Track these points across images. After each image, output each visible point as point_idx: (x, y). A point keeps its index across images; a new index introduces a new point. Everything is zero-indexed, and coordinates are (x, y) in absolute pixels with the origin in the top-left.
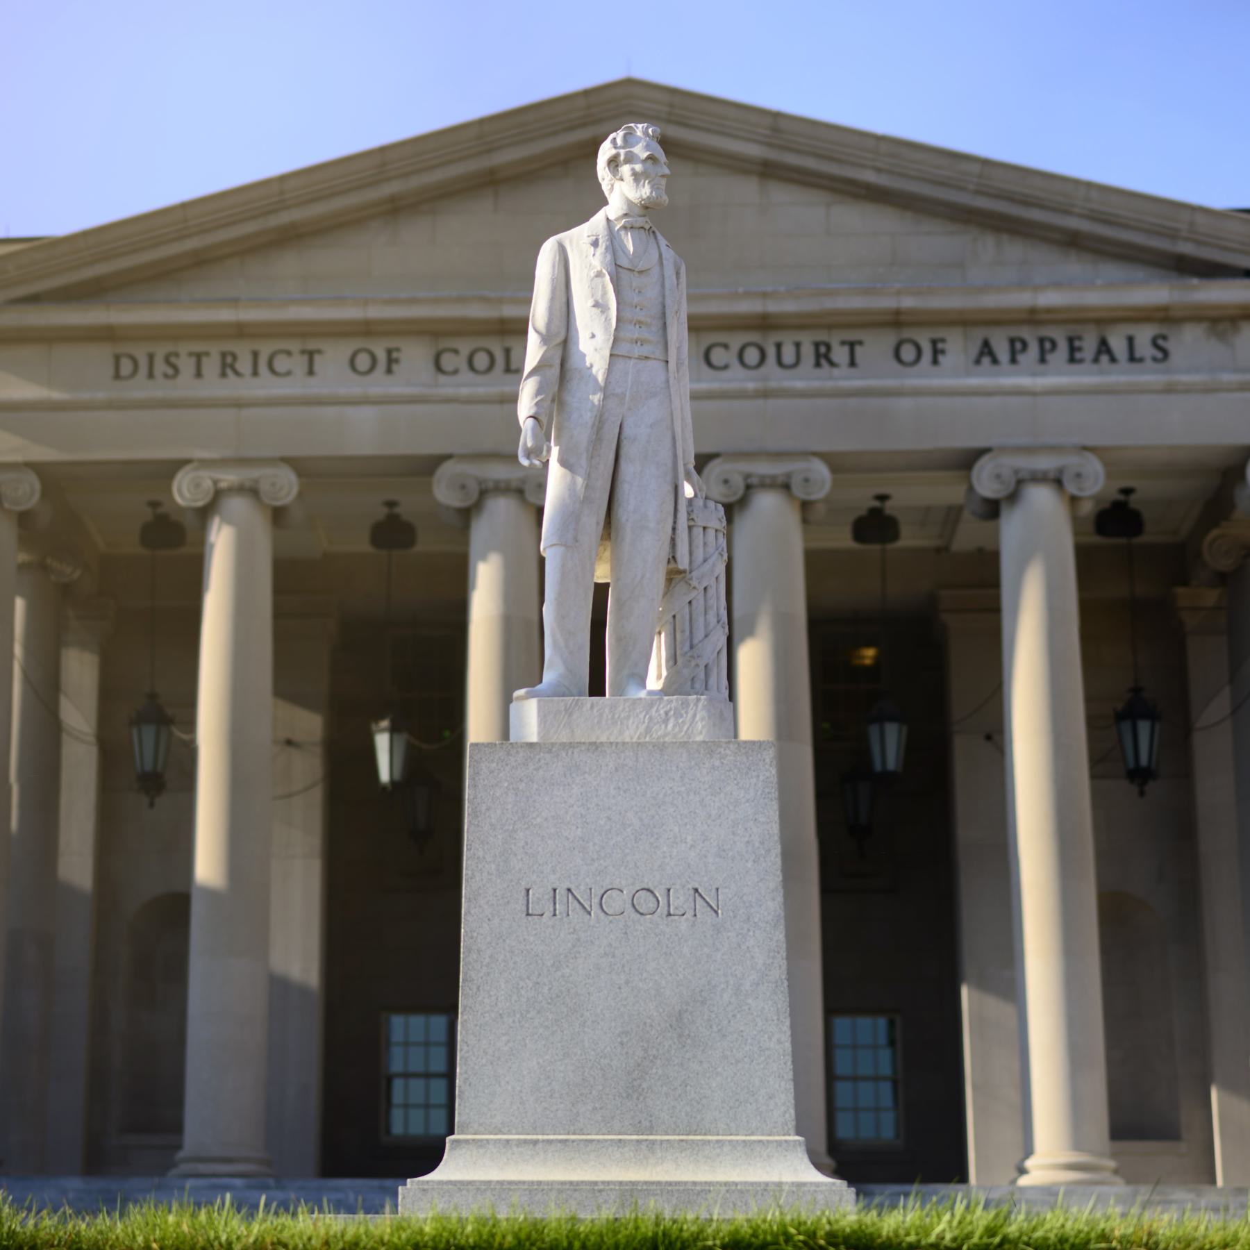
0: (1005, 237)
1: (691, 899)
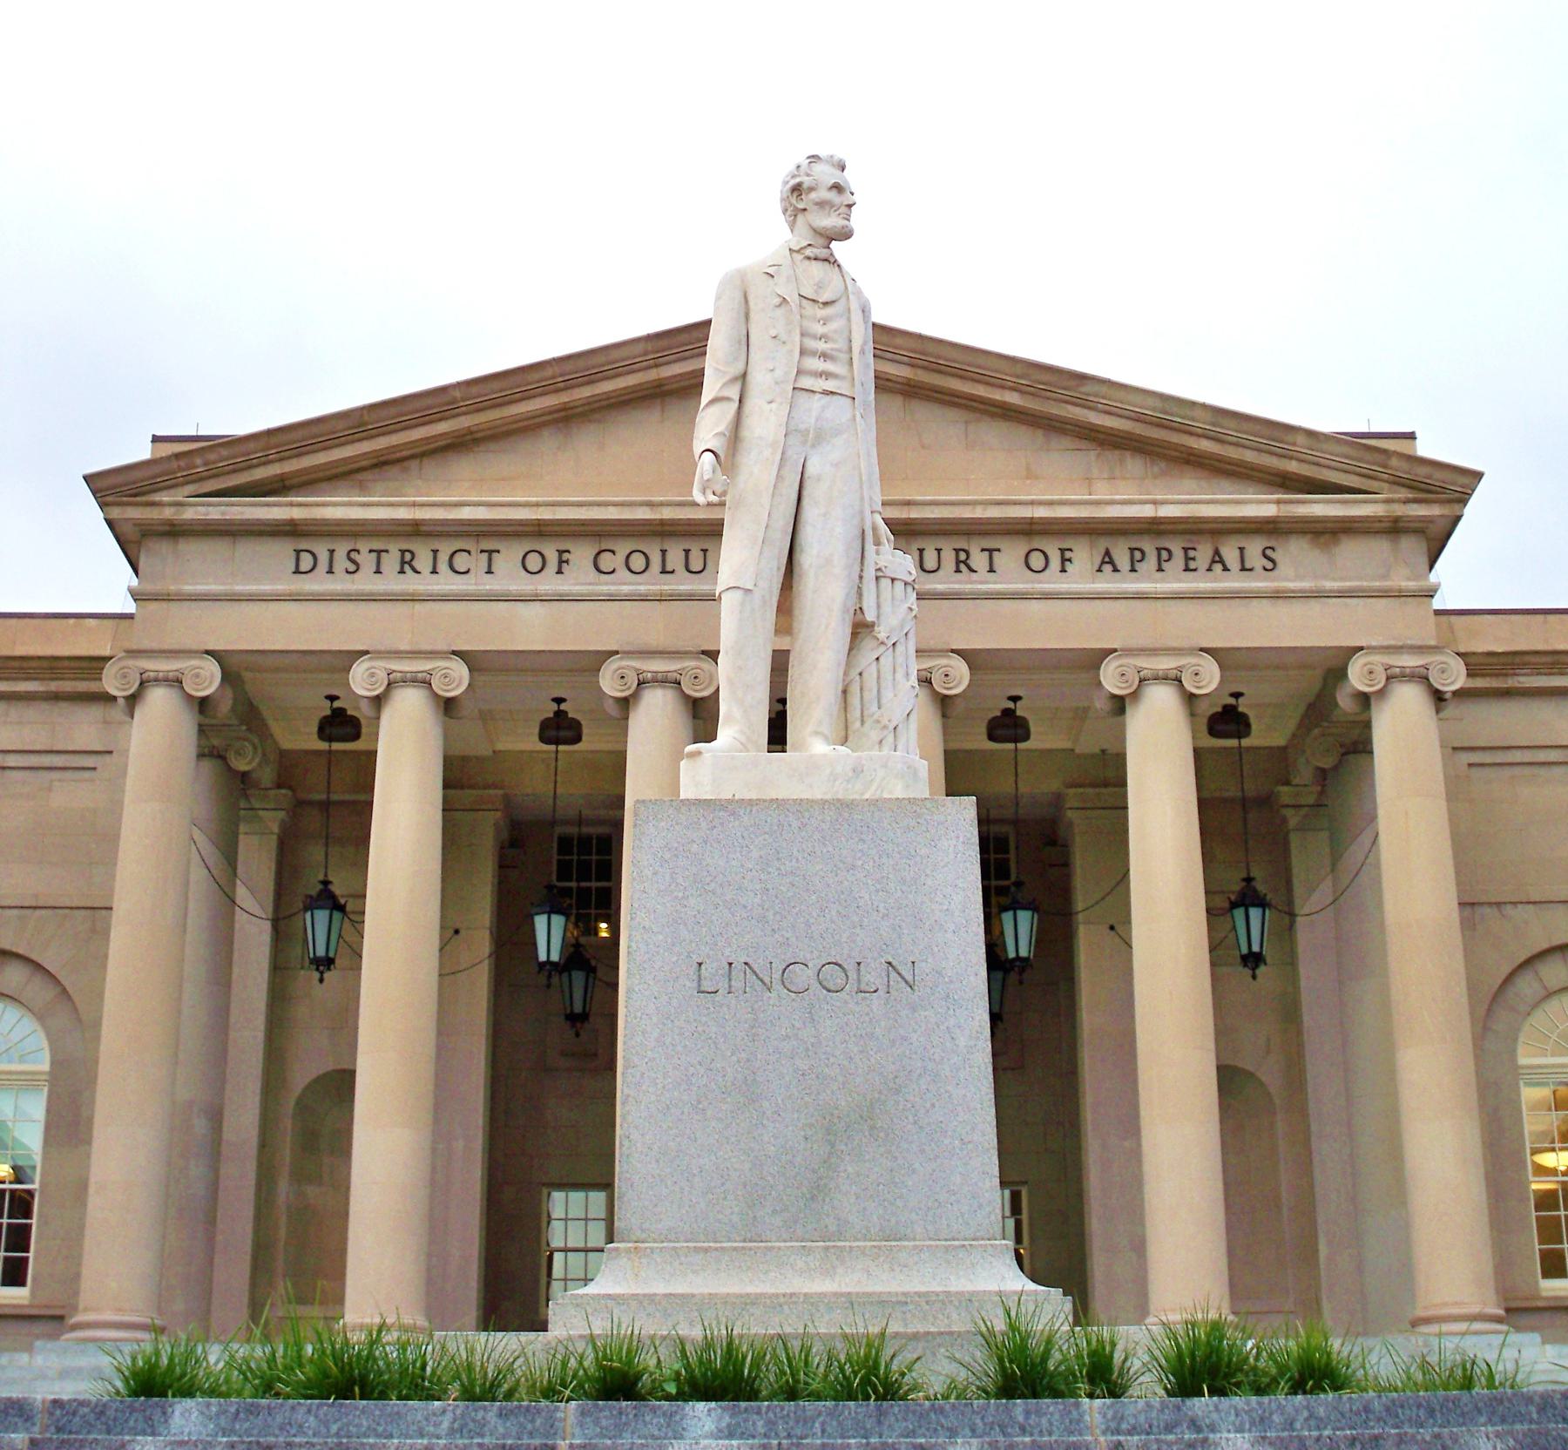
0: (1128, 454)
1: (884, 974)
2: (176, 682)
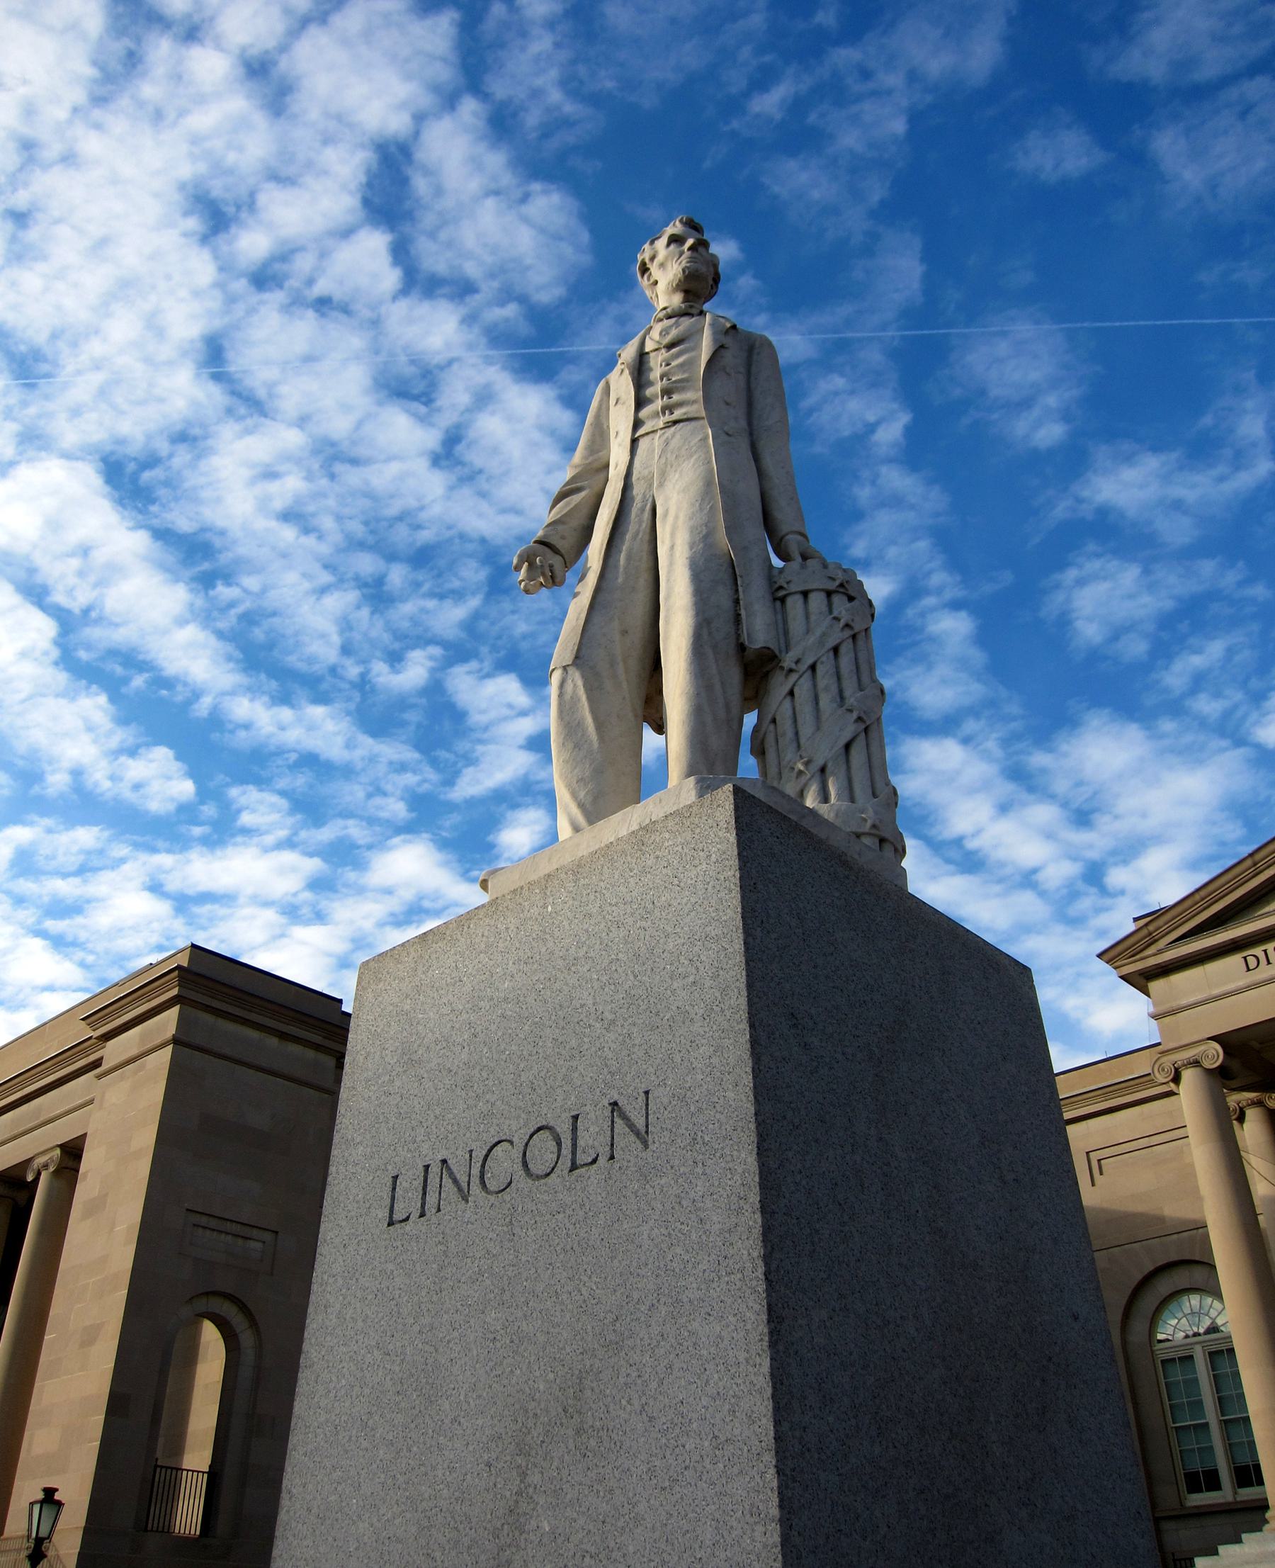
2: (1196, 1063)
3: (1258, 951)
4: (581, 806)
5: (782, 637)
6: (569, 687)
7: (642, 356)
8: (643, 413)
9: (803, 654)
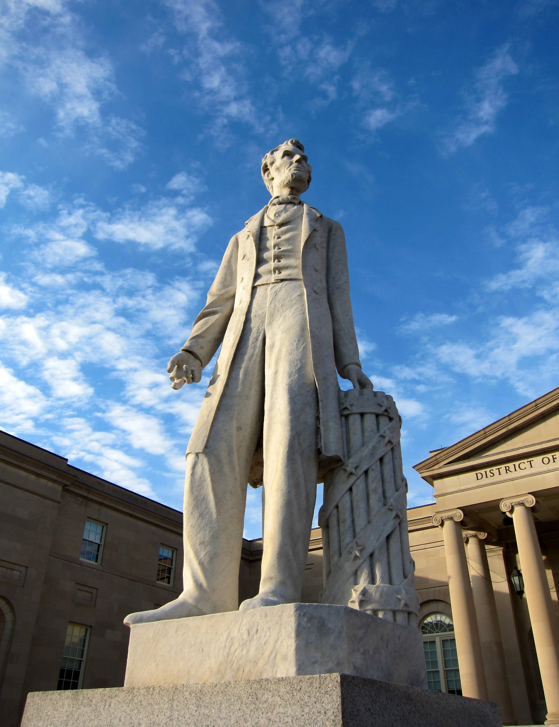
2: (451, 518)
3: (483, 471)
4: (201, 564)
5: (345, 444)
6: (199, 469)
7: (262, 229)
8: (261, 270)
9: (360, 462)
